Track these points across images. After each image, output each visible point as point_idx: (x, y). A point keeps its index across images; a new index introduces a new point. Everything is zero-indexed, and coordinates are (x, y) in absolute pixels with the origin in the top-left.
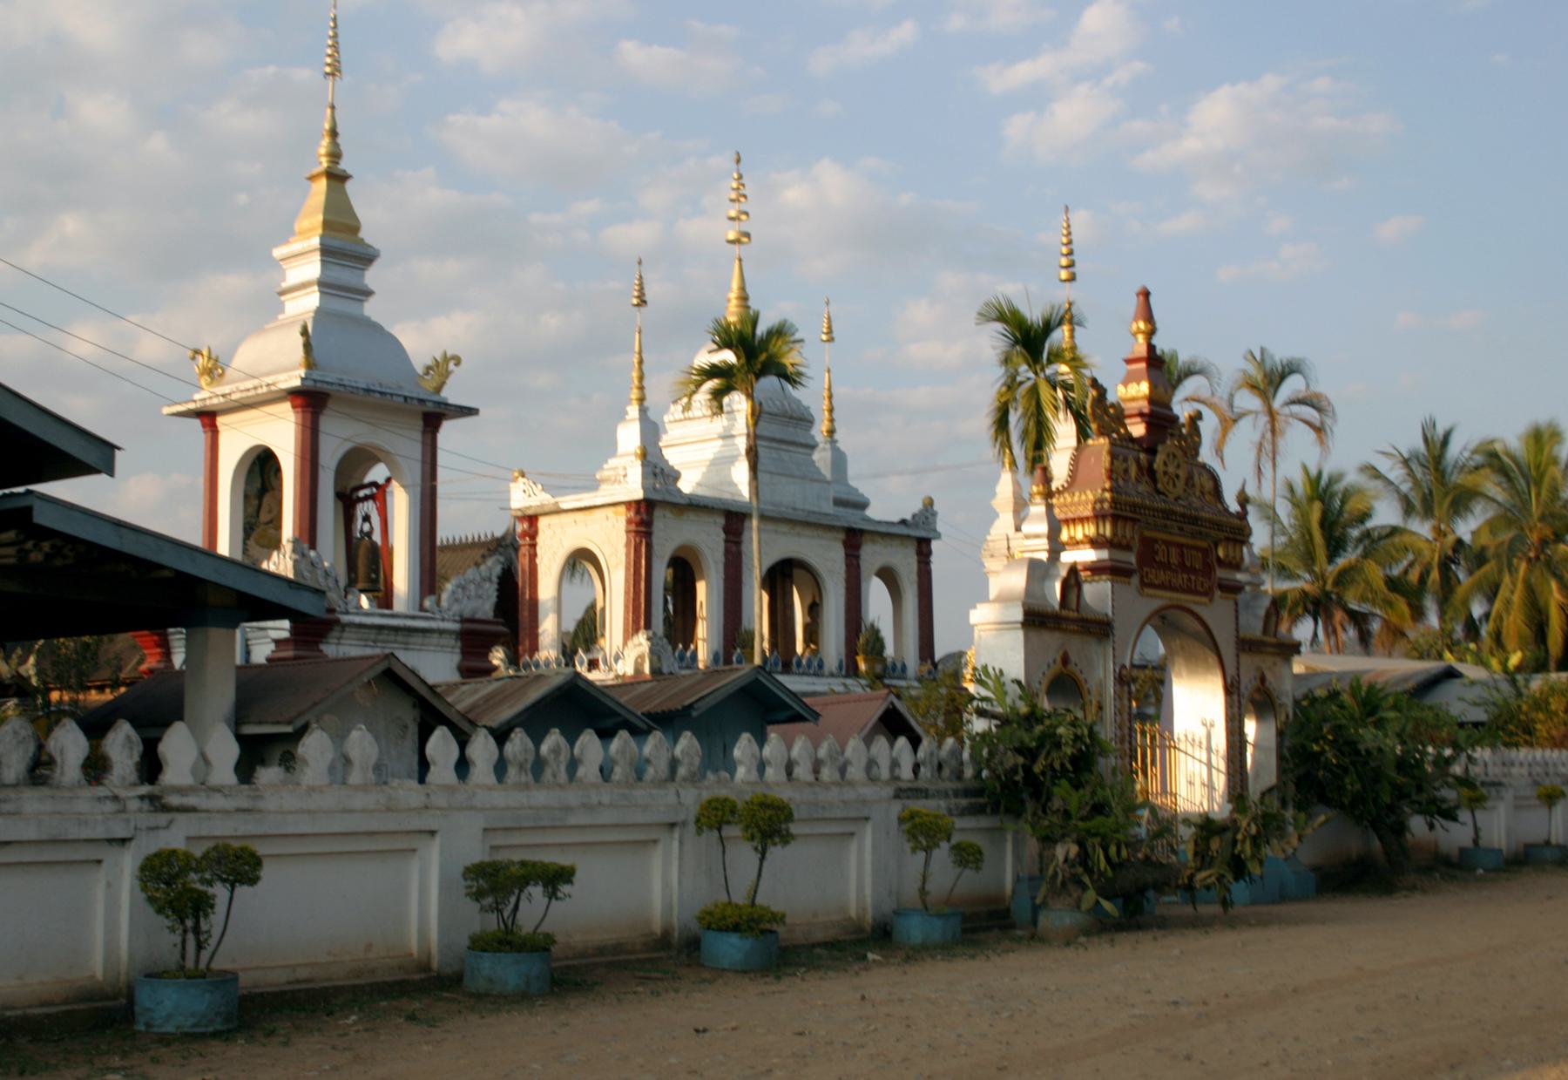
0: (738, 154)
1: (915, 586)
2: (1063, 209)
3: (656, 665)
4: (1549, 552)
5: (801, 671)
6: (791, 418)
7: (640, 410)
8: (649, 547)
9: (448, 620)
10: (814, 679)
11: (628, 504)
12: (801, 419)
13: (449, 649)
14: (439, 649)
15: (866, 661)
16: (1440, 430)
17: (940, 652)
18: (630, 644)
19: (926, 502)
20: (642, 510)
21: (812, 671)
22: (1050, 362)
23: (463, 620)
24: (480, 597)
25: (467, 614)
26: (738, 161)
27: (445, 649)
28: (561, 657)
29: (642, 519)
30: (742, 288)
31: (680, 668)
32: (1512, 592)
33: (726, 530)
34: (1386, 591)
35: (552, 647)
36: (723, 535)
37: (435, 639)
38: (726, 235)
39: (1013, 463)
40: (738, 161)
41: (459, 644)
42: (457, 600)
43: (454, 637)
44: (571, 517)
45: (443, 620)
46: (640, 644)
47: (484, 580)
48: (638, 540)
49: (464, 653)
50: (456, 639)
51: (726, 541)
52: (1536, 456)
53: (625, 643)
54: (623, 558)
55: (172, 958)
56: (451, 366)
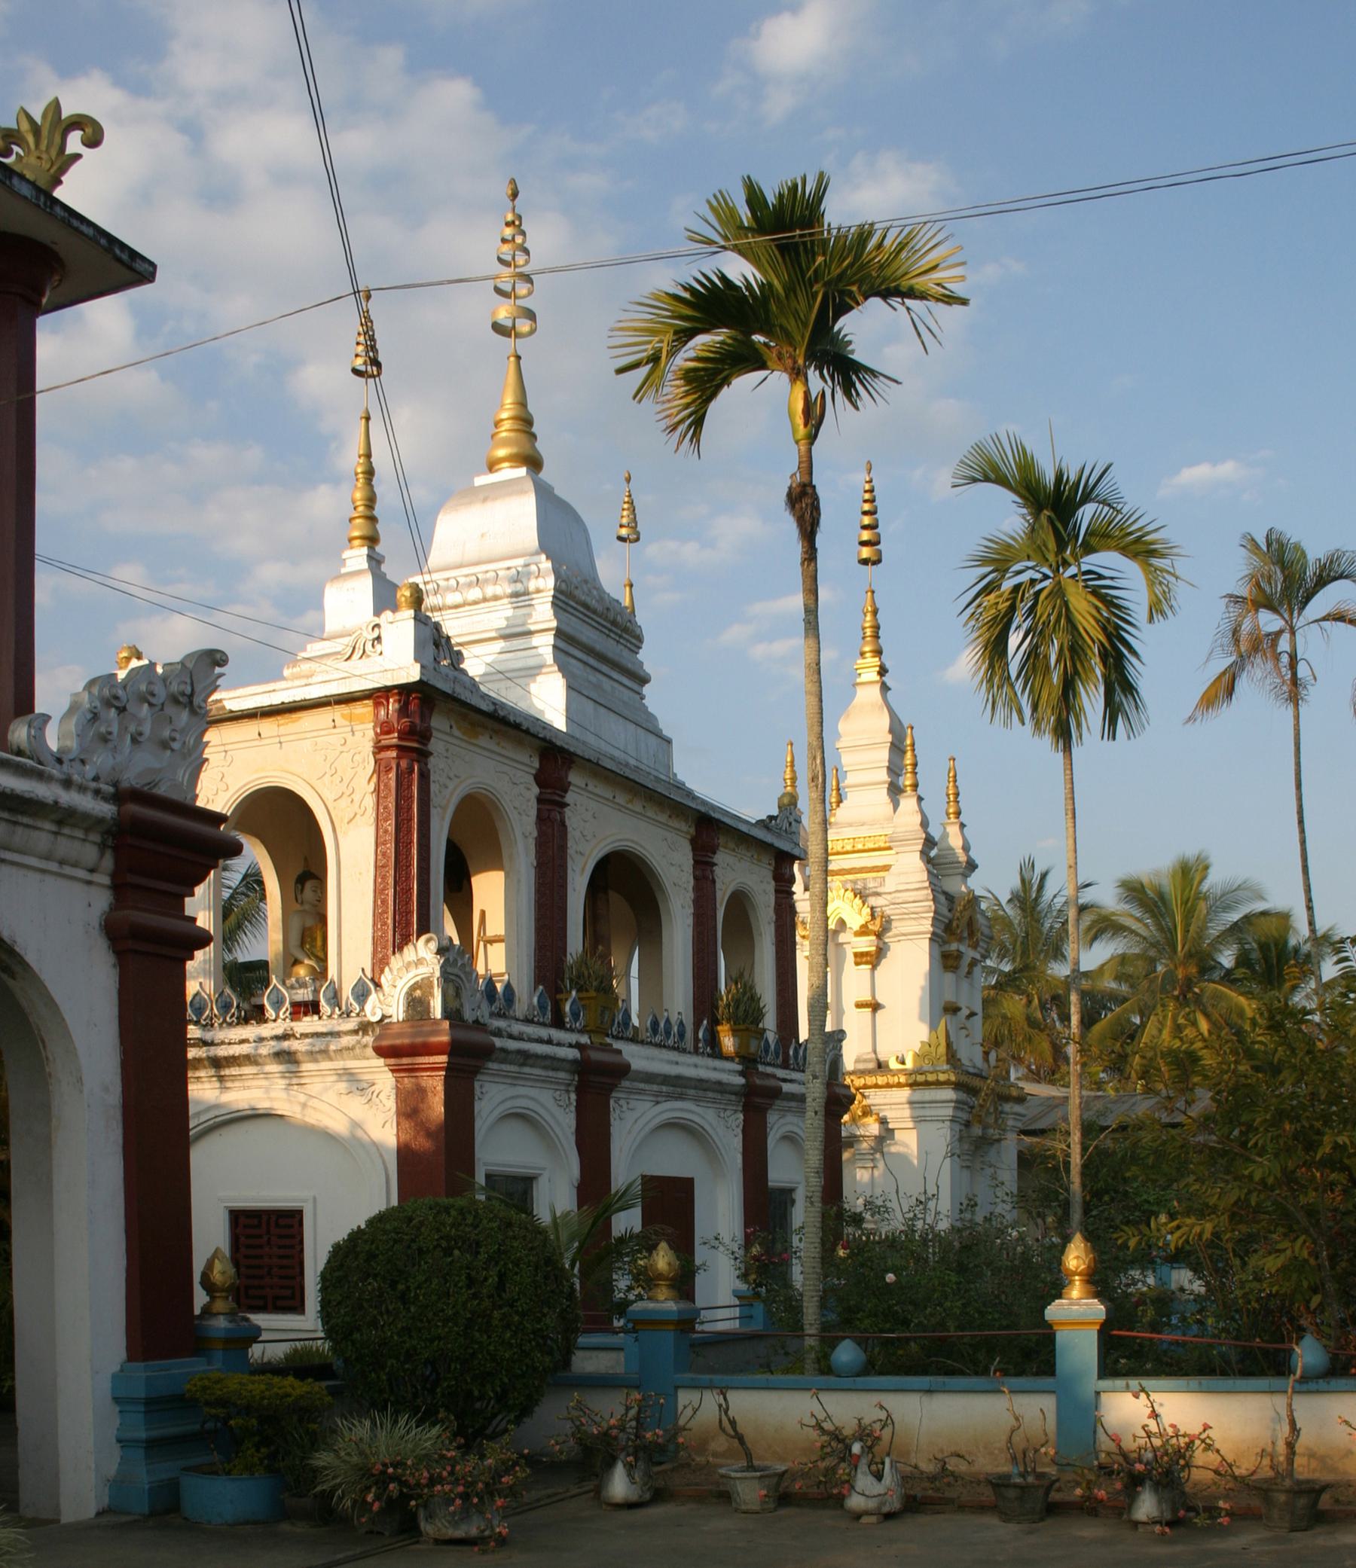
0: (513, 181)
1: (772, 927)
2: (864, 466)
3: (454, 1005)
4: (1196, 990)
5: (658, 1039)
6: (614, 623)
7: (370, 557)
8: (424, 777)
9: (82, 789)
10: (673, 1056)
11: (378, 695)
12: (626, 630)
13: (81, 874)
14: (53, 866)
15: (735, 1032)
16: (1038, 870)
17: (1319, 933)
18: (396, 962)
19: (786, 801)
20: (413, 707)
21: (670, 1042)
22: (1088, 549)
23: (121, 796)
24: (165, 745)
25: (131, 778)
26: (515, 195)
27: (67, 870)
28: (228, 991)
29: (413, 725)
30: (522, 403)
31: (492, 1015)
32: (1160, 1031)
33: (540, 779)
34: (1026, 1027)
35: (206, 974)
36: (536, 790)
37: (42, 837)
38: (494, 313)
39: (1020, 712)
40: (515, 195)
41: (108, 862)
42: (105, 739)
43: (95, 837)
44: (250, 728)
45: (67, 783)
46: (419, 962)
47: (175, 700)
48: (404, 764)
49: (118, 887)
50: (102, 847)
51: (540, 800)
52: (1183, 891)
53: (380, 963)
54: (370, 802)
55: (481, 597)
56: (74, 142)
